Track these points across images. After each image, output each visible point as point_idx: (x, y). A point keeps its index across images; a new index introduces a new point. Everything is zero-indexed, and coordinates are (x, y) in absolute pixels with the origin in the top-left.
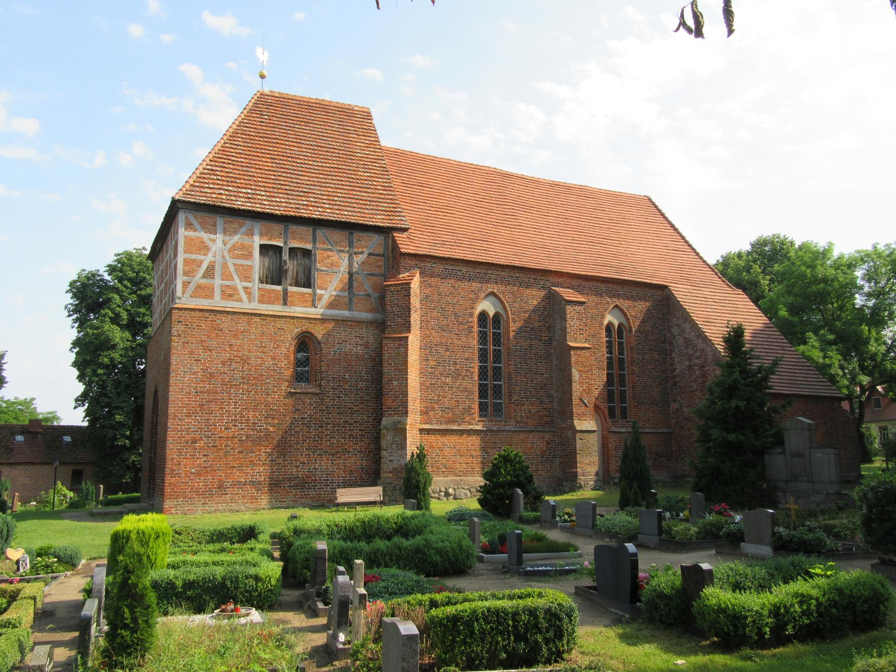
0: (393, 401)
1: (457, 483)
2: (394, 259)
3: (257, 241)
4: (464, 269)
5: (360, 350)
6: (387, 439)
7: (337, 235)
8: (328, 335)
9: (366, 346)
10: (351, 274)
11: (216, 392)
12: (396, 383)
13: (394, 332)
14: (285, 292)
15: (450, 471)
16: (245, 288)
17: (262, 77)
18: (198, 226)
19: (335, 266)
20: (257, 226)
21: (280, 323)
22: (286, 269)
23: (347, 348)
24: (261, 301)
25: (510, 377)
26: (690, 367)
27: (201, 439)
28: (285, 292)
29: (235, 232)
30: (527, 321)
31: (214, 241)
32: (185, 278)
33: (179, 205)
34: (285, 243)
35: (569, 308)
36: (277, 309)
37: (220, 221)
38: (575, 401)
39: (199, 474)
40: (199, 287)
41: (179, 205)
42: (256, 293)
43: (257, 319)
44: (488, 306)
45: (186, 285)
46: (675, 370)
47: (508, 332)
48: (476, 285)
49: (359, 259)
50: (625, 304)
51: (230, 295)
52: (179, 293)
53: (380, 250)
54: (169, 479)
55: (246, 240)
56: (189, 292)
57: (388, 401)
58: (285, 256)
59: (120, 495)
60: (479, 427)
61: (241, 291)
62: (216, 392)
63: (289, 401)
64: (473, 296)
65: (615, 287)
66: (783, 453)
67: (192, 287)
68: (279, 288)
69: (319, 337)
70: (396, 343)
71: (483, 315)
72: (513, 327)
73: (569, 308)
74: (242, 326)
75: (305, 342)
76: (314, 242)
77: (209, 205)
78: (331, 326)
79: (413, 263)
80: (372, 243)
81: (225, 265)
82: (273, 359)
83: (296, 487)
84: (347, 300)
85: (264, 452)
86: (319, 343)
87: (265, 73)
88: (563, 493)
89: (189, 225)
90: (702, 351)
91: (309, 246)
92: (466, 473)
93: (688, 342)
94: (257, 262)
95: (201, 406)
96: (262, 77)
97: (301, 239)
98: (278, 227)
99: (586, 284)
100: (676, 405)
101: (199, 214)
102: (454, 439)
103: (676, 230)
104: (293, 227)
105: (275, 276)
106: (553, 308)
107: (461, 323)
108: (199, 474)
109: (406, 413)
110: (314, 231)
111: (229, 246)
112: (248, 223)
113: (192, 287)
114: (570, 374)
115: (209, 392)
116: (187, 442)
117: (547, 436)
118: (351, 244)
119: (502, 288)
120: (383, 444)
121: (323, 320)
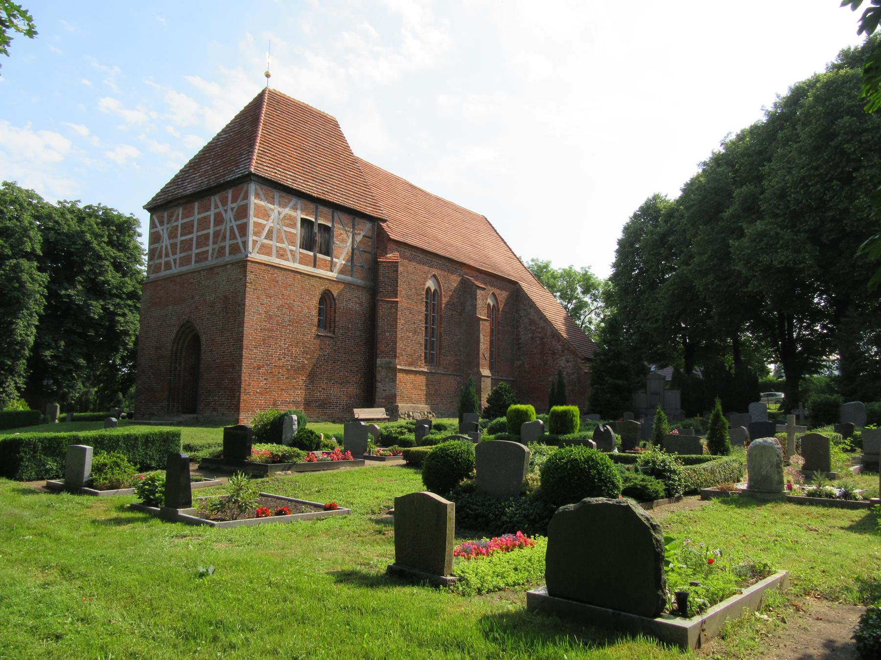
0: (386, 347)
1: (414, 408)
2: (380, 239)
3: (300, 215)
4: (421, 256)
5: (357, 307)
6: (381, 374)
7: (346, 218)
8: (340, 294)
9: (361, 304)
10: (353, 249)
11: (273, 330)
12: (388, 334)
13: (386, 297)
14: (315, 256)
15: (410, 400)
16: (291, 251)
17: (268, 76)
18: (263, 197)
19: (345, 241)
20: (300, 203)
21: (313, 281)
22: (316, 240)
23: (351, 305)
24: (300, 263)
25: (441, 336)
26: (532, 338)
27: (263, 366)
28: (315, 256)
29: (285, 206)
30: (451, 297)
31: (273, 210)
32: (255, 238)
33: (252, 178)
34: (316, 219)
35: (479, 292)
36: (309, 269)
37: (277, 195)
38: (481, 356)
39: (261, 394)
40: (263, 246)
41: (252, 178)
42: (298, 256)
43: (299, 276)
44: (430, 284)
45: (255, 242)
46: (520, 339)
47: (441, 304)
48: (426, 268)
49: (359, 238)
50: (497, 292)
51: (282, 255)
52: (250, 249)
53: (370, 234)
54: (243, 397)
55: (293, 213)
56: (256, 249)
57: (382, 347)
58: (316, 229)
59: (88, 414)
60: (425, 370)
61: (289, 253)
62: (273, 330)
63: (317, 342)
64: (424, 276)
65: (494, 280)
66: (646, 392)
67: (258, 245)
68: (311, 254)
69: (335, 295)
70: (389, 305)
71: (429, 289)
72: (445, 300)
73: (479, 292)
74: (290, 281)
75: (326, 298)
76: (333, 221)
77: (273, 182)
78: (341, 287)
79: (394, 247)
80: (365, 228)
81: (279, 231)
82: (308, 309)
83: (319, 407)
84: (350, 268)
85: (301, 380)
86: (334, 299)
87: (271, 73)
88: (161, 434)
89: (257, 195)
90: (543, 328)
91: (330, 225)
92: (418, 402)
93: (532, 322)
94: (298, 231)
95: (264, 340)
96: (268, 76)
97: (325, 218)
98: (312, 206)
99: (480, 276)
100: (519, 363)
101: (264, 187)
102: (411, 377)
103: (505, 243)
104: (321, 208)
105: (308, 244)
106: (466, 291)
107: (418, 295)
108: (261, 394)
109: (395, 356)
110: (317, 208)
111: (282, 216)
112: (294, 200)
113: (258, 245)
114: (479, 337)
115: (268, 330)
116: (254, 368)
117: (458, 378)
118: (353, 228)
119: (440, 272)
120: (378, 377)
121: (338, 282)
